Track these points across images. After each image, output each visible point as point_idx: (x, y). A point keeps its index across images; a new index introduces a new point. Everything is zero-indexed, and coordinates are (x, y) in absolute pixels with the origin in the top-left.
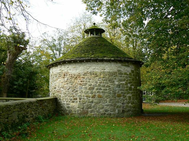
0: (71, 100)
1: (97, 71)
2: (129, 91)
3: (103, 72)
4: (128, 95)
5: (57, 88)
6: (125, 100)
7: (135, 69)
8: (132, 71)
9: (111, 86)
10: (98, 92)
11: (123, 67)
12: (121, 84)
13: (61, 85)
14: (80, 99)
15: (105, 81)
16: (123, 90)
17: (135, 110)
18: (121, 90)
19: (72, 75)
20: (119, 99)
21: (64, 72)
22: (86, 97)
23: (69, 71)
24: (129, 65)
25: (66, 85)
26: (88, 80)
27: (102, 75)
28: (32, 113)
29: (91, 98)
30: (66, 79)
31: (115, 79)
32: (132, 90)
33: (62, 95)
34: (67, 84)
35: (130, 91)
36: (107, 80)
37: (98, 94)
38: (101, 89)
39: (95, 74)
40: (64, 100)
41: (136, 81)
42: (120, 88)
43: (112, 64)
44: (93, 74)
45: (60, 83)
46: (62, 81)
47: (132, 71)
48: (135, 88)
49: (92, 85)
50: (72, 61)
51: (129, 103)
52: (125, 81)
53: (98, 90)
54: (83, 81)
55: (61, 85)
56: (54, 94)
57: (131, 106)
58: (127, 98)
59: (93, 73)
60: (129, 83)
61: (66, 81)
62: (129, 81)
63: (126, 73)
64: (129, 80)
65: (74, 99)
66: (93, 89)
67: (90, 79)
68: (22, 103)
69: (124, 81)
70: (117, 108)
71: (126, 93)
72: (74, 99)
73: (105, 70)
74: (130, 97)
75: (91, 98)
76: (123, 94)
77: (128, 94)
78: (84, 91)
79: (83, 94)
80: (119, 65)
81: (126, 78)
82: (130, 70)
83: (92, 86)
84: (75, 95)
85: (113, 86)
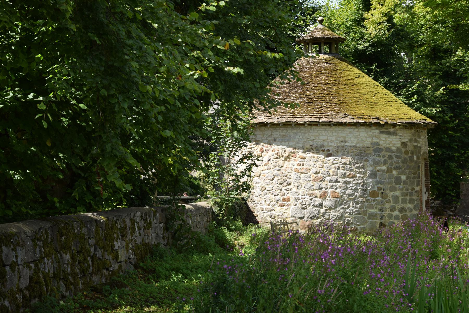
2: (394, 185)
3: (343, 147)
8: (403, 143)
11: (384, 137)
12: (378, 171)
32: (402, 184)
35: (397, 186)
39: (326, 150)
43: (288, 129)
52: (387, 165)
60: (396, 169)
65: (284, 200)
69: (384, 165)
70: (369, 218)
72: (284, 200)
73: (346, 142)
74: (396, 199)
76: (382, 191)
77: (391, 191)
82: (399, 142)
84: (286, 192)
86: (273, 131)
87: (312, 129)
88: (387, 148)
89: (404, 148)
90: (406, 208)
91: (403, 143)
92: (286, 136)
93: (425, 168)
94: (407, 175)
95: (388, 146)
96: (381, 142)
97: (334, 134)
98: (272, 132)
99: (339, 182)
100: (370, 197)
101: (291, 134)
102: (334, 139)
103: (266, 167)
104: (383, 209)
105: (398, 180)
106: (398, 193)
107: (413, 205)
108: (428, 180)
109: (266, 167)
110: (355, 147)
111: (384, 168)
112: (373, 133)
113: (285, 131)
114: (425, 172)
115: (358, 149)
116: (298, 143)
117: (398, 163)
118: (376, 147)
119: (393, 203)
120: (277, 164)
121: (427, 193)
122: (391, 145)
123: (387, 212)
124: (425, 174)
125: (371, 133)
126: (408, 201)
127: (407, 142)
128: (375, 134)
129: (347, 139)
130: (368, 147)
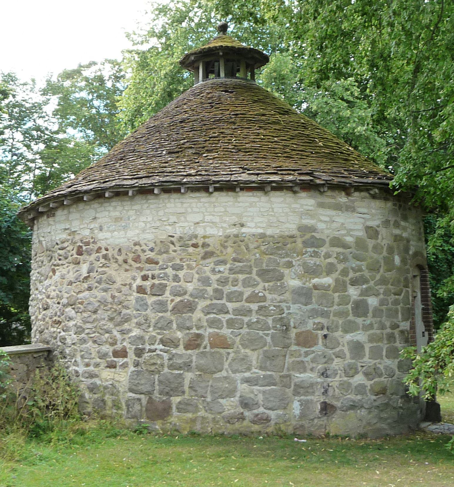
0: (103, 356)
1: (210, 231)
2: (351, 317)
3: (236, 236)
4: (349, 337)
5: (55, 308)
6: (336, 360)
7: (386, 223)
8: (368, 229)
9: (269, 296)
10: (212, 323)
11: (326, 214)
12: (316, 287)
13: (66, 295)
14: (139, 353)
15: (241, 277)
16: (324, 314)
17: (387, 405)
18: (314, 313)
19: (107, 250)
20: (307, 354)
21: (77, 238)
22: (161, 347)
23: (101, 236)
24: (353, 201)
25: (87, 293)
26: (170, 271)
27: (230, 250)
28: (106, 398)
29: (180, 350)
30: (84, 268)
31: (289, 265)
32: (370, 314)
33: (71, 337)
34: (90, 289)
35: (360, 320)
36: (250, 273)
37: (211, 330)
38: (224, 310)
39: (200, 243)
40: (79, 359)
41: (388, 275)
42: (309, 307)
43: (125, 203)
44: (195, 246)
45: (65, 286)
46: (71, 276)
47: (372, 232)
48: (384, 307)
49: (185, 293)
50: (104, 190)
51: (351, 371)
52: (335, 275)
53: (212, 316)
54: (153, 277)
55: (66, 295)
56: (41, 332)
57: (363, 386)
58: (346, 349)
59: (190, 243)
60: (354, 282)
61: (86, 278)
62: (351, 275)
63: (338, 239)
64: (355, 270)
65: (116, 354)
66: (190, 307)
67: (181, 268)
68: (318, 339)
69: (328, 275)
70: (296, 393)
71: (337, 327)
72: (116, 354)
73: (242, 225)
74: (357, 348)
75: (180, 350)
76: (325, 332)
77: (346, 331)
78: (153, 316)
79: (152, 332)
80: (307, 201)
81: (341, 261)
82: (360, 227)
83: (187, 297)
84: (119, 336)
85: (279, 298)
86: (98, 210)
87: (172, 200)
88: (335, 237)
89: (370, 238)
90: (381, 367)
91: (368, 229)
92: (121, 219)
93: (421, 284)
94: (382, 296)
95: (337, 234)
96: (321, 226)
97: (216, 209)
98: (97, 212)
99: (227, 312)
100: (298, 344)
101: (131, 213)
102: (217, 220)
103: (86, 285)
104: (329, 372)
105: (360, 308)
106: (360, 336)
107: (396, 361)
108: (428, 309)
109: (86, 285)
110: (263, 236)
111: (328, 280)
112: (302, 205)
113: (119, 208)
114: (422, 293)
115: (268, 239)
116: (144, 231)
117: (360, 270)
118: (308, 236)
119: (352, 358)
120: (104, 277)
121: (426, 333)
122: (343, 232)
123: (337, 378)
124: (422, 297)
125: (297, 206)
126: (384, 353)
127: (378, 226)
128: (305, 207)
129: (244, 220)
130: (292, 237)
